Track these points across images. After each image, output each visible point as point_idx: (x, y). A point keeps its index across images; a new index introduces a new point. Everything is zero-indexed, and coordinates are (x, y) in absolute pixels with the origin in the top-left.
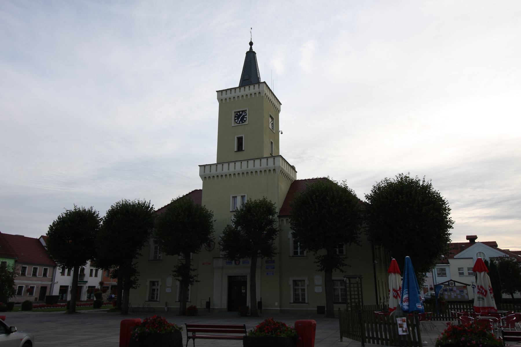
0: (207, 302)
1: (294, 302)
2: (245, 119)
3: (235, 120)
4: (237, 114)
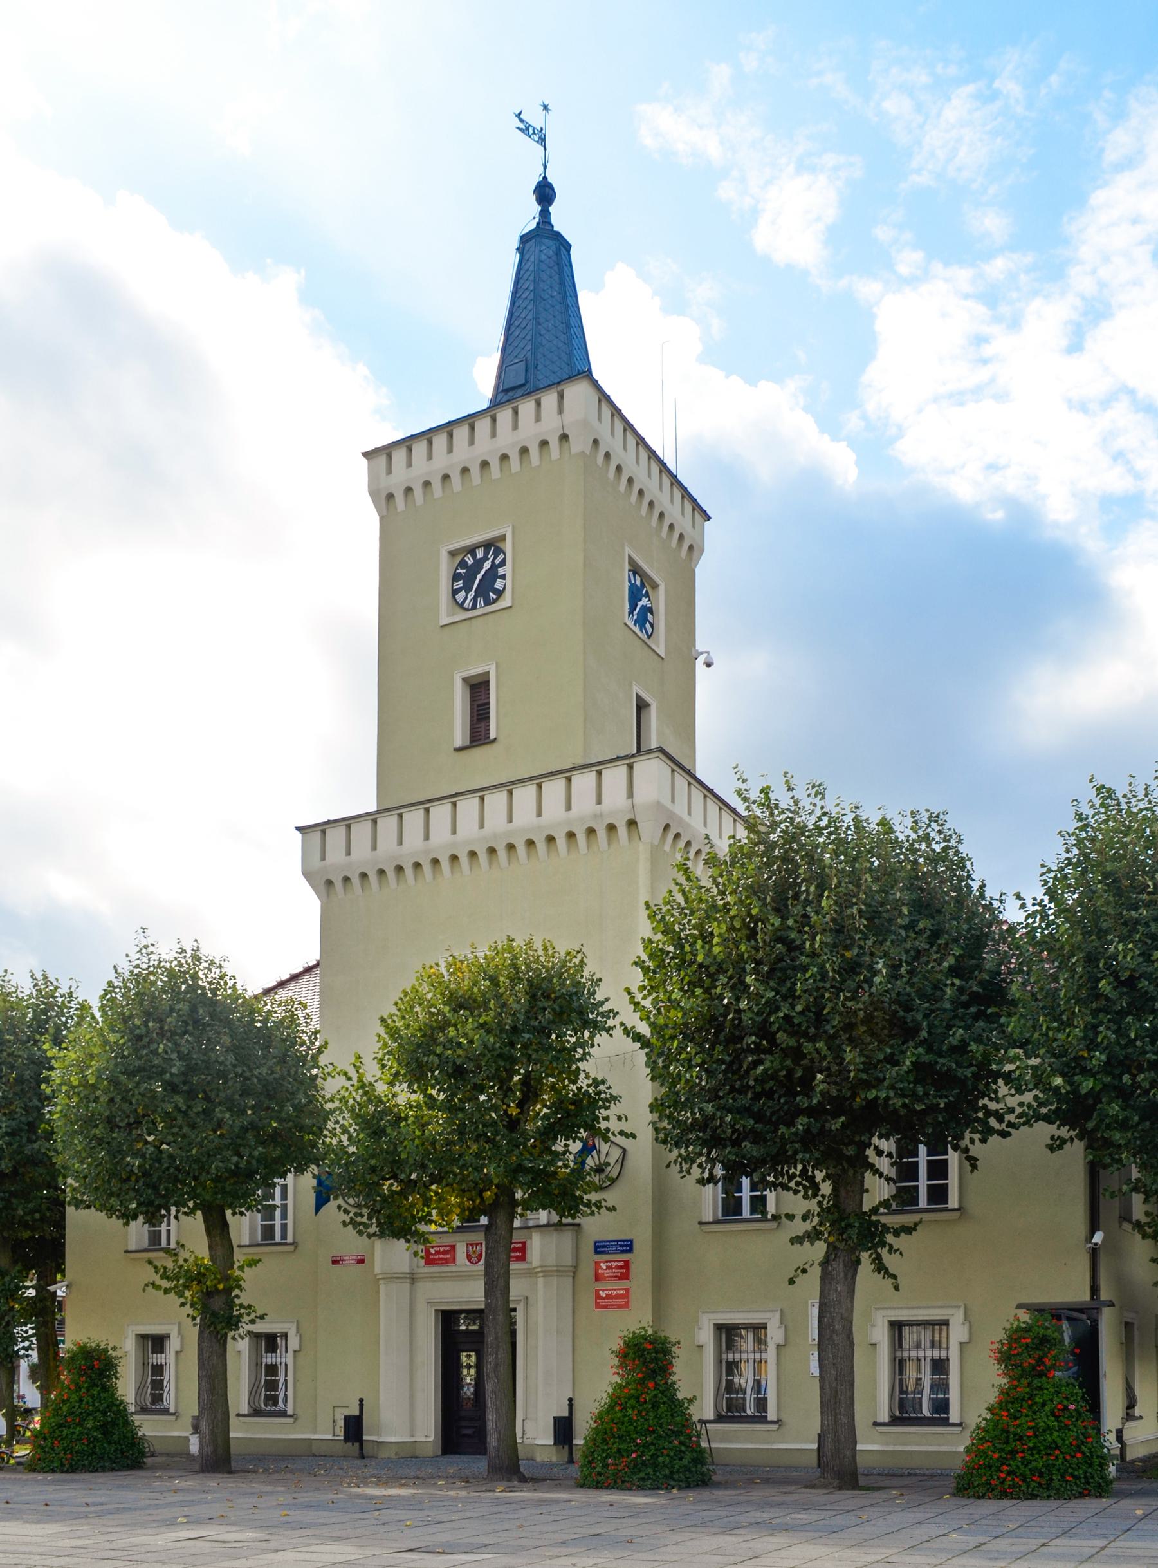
0: (347, 1419)
1: (895, 1421)
2: (499, 584)
3: (455, 592)
4: (463, 564)
